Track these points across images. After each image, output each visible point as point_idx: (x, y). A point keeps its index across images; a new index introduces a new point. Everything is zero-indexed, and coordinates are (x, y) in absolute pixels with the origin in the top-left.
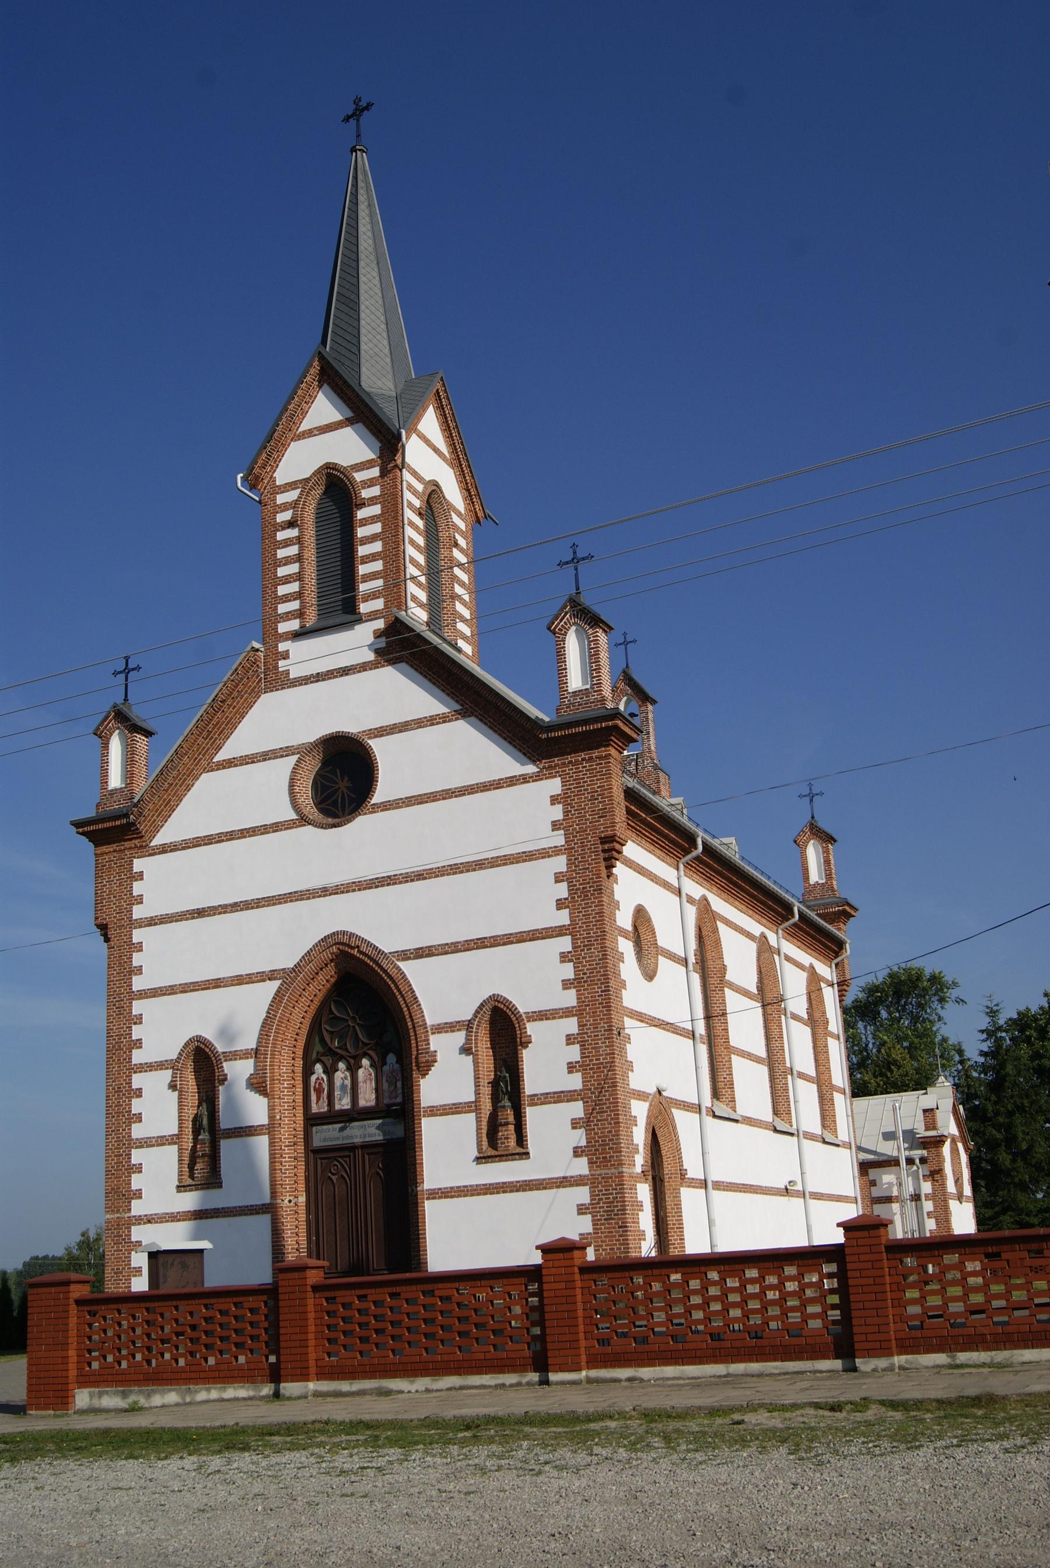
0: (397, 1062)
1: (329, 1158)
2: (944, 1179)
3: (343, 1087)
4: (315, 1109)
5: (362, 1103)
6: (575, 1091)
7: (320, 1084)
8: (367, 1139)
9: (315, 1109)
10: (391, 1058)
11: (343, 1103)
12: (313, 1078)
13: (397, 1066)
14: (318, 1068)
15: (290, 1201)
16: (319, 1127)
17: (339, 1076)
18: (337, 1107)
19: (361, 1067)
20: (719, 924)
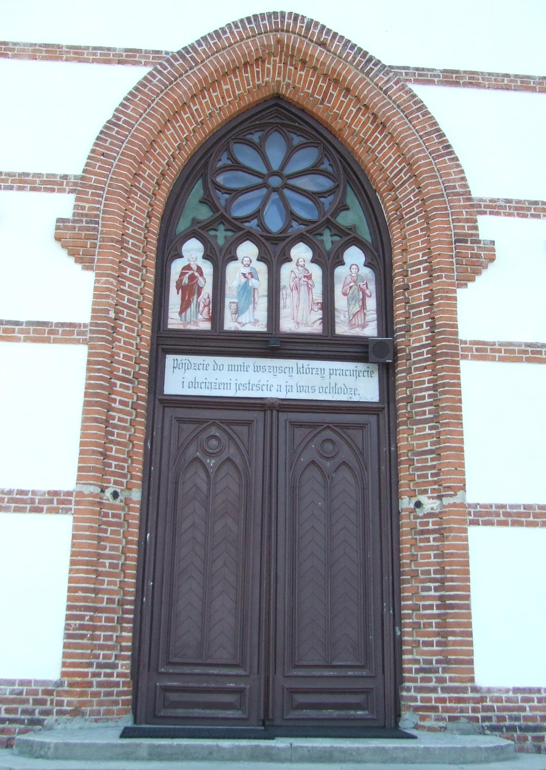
0: (260, 259)
1: (199, 422)
2: (528, 693)
3: (246, 291)
4: (175, 321)
5: (287, 325)
6: (474, 358)
7: (192, 278)
8: (291, 396)
9: (175, 321)
10: (354, 256)
11: (251, 319)
12: (176, 267)
13: (367, 272)
14: (193, 249)
15: (115, 495)
16: (180, 357)
17: (234, 273)
18: (230, 325)
19: (289, 260)
20: (421, 91)
